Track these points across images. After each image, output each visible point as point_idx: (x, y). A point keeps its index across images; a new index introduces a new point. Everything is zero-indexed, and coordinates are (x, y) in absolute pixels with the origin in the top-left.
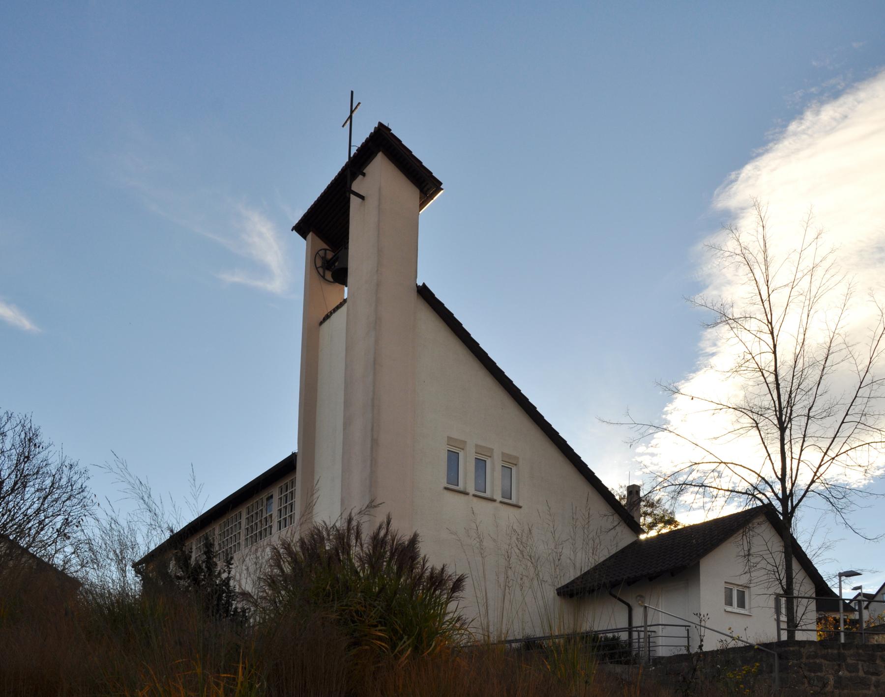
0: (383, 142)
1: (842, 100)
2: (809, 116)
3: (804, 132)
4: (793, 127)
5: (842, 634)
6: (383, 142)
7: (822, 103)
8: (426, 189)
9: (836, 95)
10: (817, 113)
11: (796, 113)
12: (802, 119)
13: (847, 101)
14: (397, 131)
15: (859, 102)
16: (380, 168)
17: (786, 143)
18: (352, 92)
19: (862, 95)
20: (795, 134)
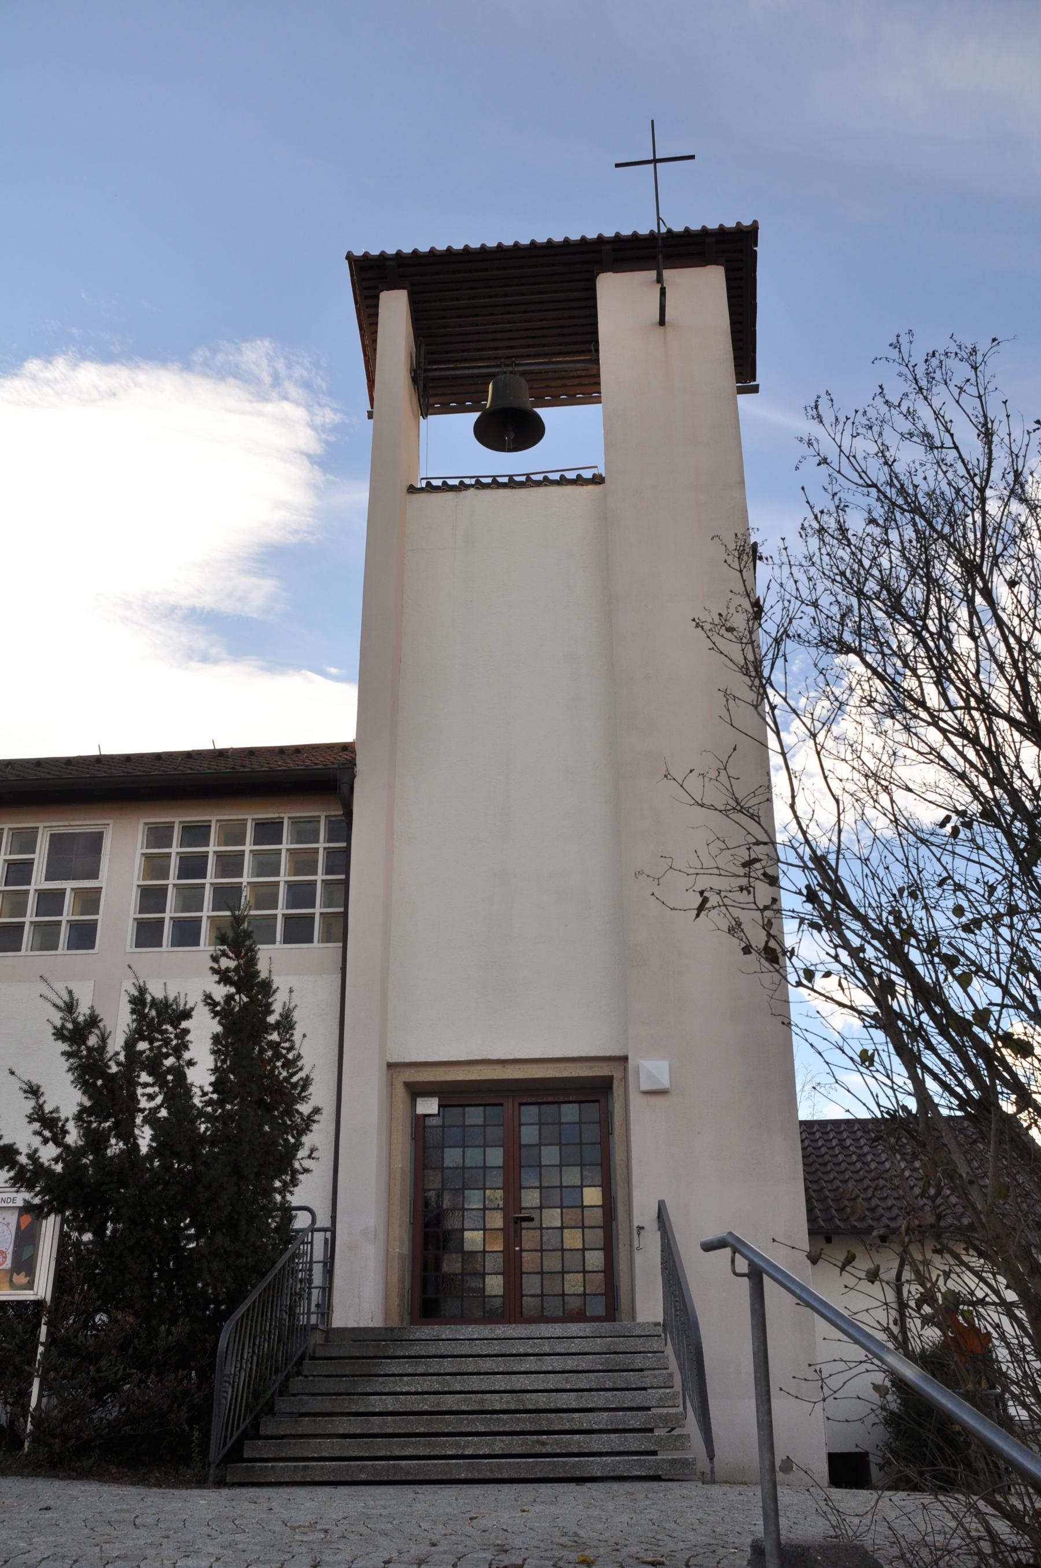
0: (732, 251)
1: (112, 369)
2: (60, 364)
3: (48, 382)
4: (33, 366)
5: (43, 1338)
6: (732, 251)
7: (85, 357)
8: (395, 306)
9: (105, 357)
10: (75, 366)
11: (47, 353)
12: (50, 362)
13: (117, 376)
14: (762, 250)
15: (136, 385)
16: (702, 289)
17: (17, 383)
18: (692, 157)
19: (141, 377)
20: (34, 378)
